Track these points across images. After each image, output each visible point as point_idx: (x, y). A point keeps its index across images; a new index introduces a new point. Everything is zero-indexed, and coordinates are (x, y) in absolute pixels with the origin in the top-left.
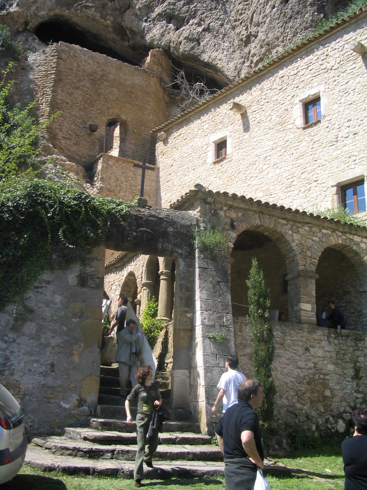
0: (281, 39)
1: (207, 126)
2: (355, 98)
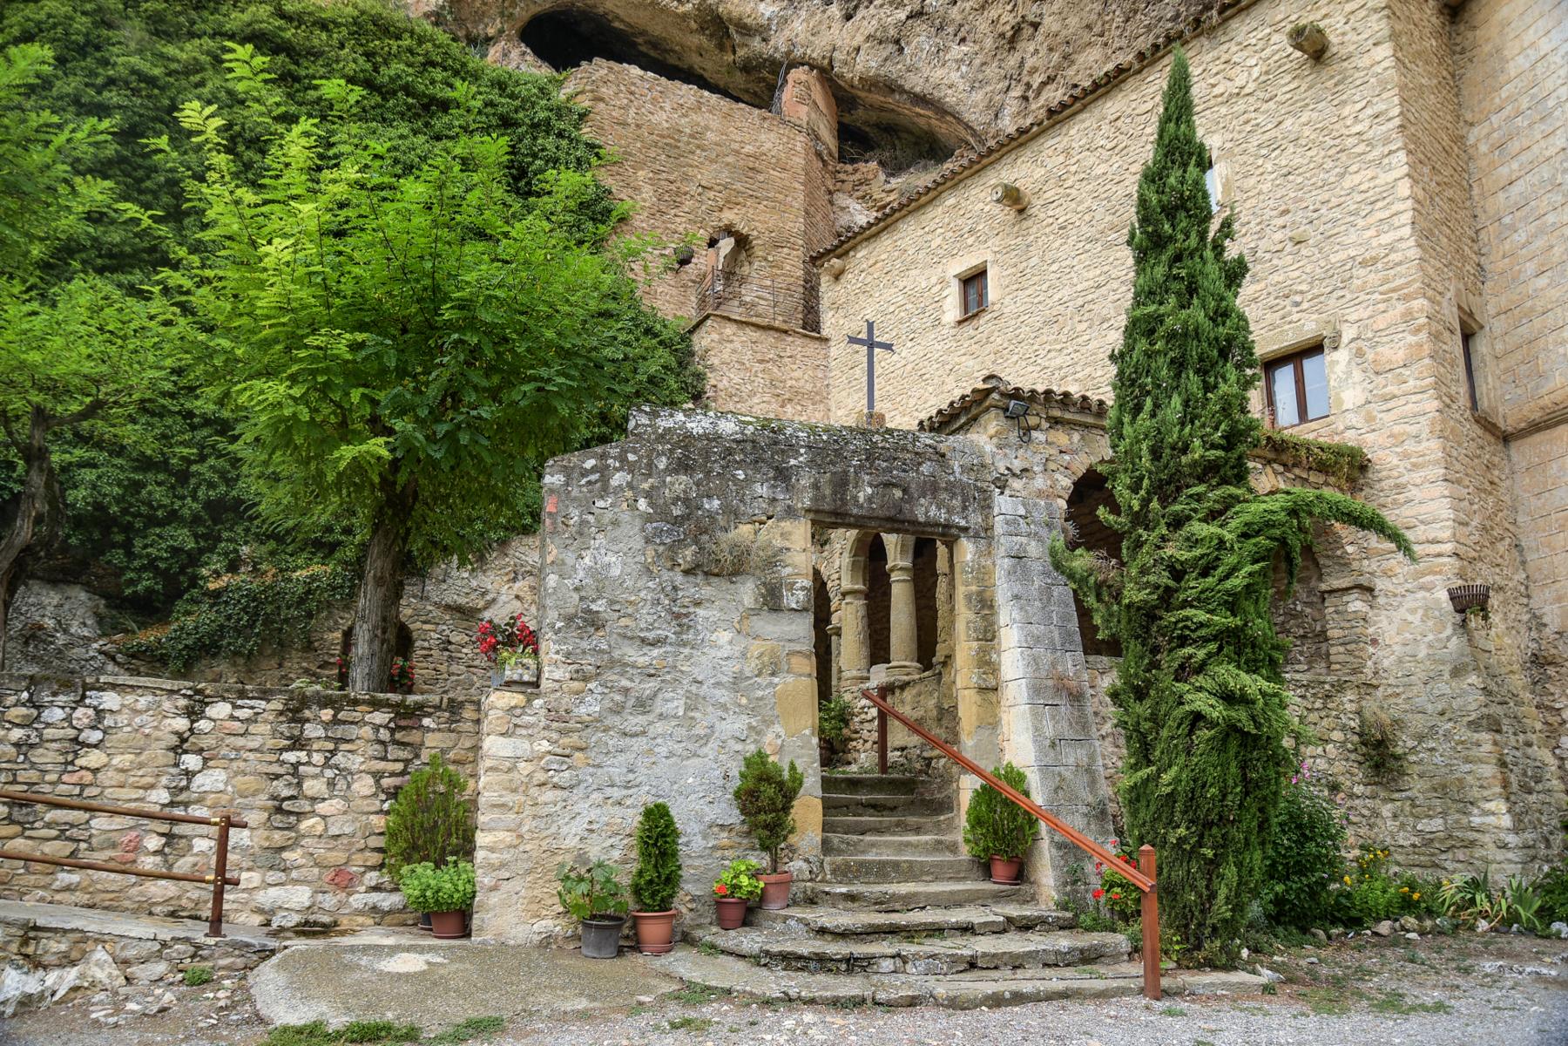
0: (1097, 30)
1: (938, 241)
2: (1297, 161)
